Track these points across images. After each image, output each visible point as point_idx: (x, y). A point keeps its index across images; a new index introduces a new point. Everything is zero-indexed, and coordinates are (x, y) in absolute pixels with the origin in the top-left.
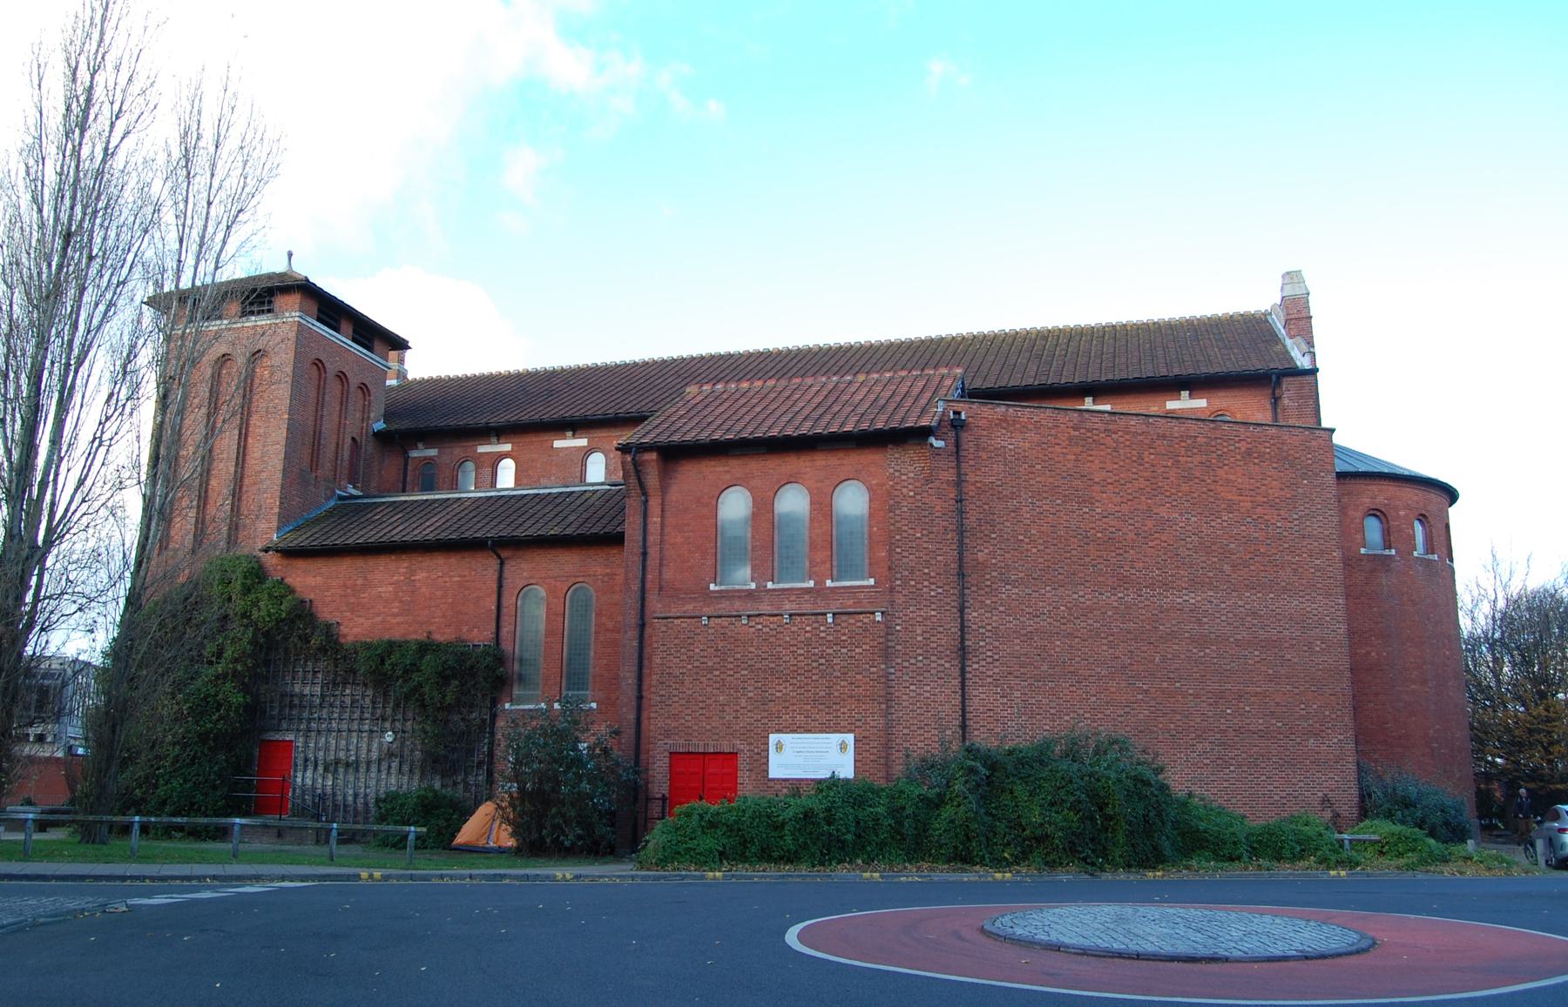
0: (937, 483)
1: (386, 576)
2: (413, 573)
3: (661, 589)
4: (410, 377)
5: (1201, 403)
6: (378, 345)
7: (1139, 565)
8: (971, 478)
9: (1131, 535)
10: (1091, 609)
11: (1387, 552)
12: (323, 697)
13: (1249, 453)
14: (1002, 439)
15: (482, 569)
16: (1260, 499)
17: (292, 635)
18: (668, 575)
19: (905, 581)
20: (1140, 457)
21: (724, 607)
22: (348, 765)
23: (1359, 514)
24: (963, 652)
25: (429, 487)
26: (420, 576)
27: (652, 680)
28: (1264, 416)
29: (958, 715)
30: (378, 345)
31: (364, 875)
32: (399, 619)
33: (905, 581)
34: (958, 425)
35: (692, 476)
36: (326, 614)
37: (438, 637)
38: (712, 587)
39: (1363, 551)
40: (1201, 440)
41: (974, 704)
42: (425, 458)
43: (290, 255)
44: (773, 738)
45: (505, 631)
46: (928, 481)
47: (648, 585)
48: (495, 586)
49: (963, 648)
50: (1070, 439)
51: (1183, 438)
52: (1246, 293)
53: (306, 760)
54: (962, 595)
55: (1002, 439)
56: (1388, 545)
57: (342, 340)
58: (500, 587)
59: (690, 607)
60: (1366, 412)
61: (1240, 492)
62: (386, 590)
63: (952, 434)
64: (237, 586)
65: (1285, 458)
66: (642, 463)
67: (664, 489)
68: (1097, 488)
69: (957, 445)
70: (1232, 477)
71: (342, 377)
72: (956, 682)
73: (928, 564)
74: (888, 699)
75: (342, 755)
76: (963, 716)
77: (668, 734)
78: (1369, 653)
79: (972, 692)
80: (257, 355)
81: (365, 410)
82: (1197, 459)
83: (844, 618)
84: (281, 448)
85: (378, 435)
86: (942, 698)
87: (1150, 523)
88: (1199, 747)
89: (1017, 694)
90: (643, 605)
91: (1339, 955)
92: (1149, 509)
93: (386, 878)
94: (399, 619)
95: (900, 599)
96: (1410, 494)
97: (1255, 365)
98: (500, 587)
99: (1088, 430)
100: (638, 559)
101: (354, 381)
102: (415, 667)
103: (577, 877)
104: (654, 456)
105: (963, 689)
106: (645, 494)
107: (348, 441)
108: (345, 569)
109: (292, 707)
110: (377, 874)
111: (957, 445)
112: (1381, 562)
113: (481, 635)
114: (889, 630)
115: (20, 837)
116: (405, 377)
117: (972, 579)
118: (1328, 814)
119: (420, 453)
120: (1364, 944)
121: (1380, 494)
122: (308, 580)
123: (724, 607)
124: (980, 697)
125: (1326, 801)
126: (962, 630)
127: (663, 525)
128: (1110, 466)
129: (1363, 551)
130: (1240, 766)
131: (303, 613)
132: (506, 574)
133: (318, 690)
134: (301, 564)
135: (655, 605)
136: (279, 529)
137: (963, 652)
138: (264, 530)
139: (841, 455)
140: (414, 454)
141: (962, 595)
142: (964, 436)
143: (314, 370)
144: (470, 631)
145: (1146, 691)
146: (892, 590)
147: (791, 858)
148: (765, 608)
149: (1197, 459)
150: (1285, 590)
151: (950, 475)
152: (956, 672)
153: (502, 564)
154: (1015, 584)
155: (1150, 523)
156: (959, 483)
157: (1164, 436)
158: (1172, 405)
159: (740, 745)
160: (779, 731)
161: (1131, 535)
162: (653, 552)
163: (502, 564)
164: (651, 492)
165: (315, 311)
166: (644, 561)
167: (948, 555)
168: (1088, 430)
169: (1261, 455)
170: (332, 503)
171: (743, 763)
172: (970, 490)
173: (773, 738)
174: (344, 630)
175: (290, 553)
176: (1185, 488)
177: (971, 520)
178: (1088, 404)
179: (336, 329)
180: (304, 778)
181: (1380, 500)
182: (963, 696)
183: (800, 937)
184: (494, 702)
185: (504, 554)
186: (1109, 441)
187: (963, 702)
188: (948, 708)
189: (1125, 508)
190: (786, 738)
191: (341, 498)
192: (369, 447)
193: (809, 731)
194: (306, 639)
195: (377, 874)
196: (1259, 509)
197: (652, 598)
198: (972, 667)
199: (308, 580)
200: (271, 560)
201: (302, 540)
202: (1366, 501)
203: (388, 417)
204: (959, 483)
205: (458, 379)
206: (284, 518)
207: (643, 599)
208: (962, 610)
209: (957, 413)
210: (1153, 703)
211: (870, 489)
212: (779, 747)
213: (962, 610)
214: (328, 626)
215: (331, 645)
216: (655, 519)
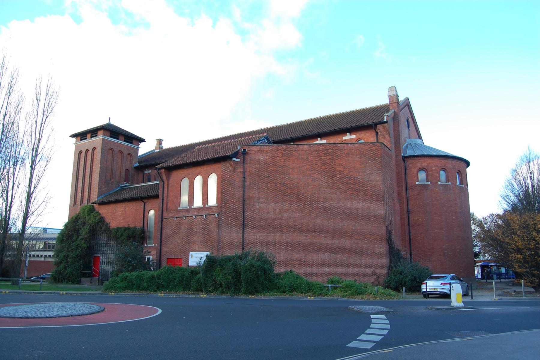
0: (237, 172)
1: (120, 208)
4: (164, 148)
5: (354, 136)
8: (248, 170)
9: (303, 185)
12: (106, 244)
13: (348, 153)
14: (259, 157)
17: (98, 227)
18: (169, 205)
19: (226, 204)
20: (307, 158)
21: (181, 214)
23: (416, 170)
24: (243, 225)
25: (149, 181)
27: (164, 236)
28: (373, 139)
29: (241, 245)
31: (4, 292)
33: (226, 204)
34: (244, 153)
35: (176, 174)
36: (107, 220)
37: (131, 226)
39: (417, 183)
43: (110, 118)
45: (145, 223)
48: (143, 210)
49: (243, 225)
51: (323, 151)
52: (368, 96)
56: (448, 181)
57: (121, 142)
58: (144, 211)
60: (437, 134)
64: (86, 214)
67: (168, 180)
68: (291, 170)
69: (244, 160)
71: (121, 152)
76: (243, 246)
77: (166, 253)
78: (418, 219)
79: (246, 238)
80: (94, 149)
82: (329, 157)
84: (98, 175)
86: (236, 240)
87: (310, 180)
89: (261, 238)
90: (162, 215)
92: (310, 175)
93: (9, 293)
95: (224, 210)
96: (438, 162)
97: (389, 122)
98: (144, 211)
101: (125, 153)
103: (67, 293)
104: (163, 170)
106: (163, 182)
107: (124, 170)
108: (111, 207)
110: (7, 292)
111: (244, 160)
112: (425, 187)
113: (140, 225)
115: (39, 283)
117: (247, 202)
118: (375, 277)
120: (102, 309)
121: (423, 162)
122: (105, 211)
124: (249, 240)
125: (374, 272)
126: (243, 218)
127: (168, 190)
128: (296, 162)
129: (417, 183)
130: (341, 260)
131: (102, 220)
132: (146, 207)
134: (102, 207)
135: (165, 214)
137: (243, 225)
138: (95, 197)
139: (210, 166)
140: (146, 172)
142: (246, 156)
147: (146, 289)
148: (190, 214)
149: (329, 157)
153: (145, 204)
154: (262, 203)
155: (310, 180)
156: (244, 172)
157: (316, 151)
158: (345, 138)
159: (183, 256)
161: (303, 185)
162: (165, 199)
163: (145, 204)
166: (163, 202)
167: (240, 195)
169: (352, 154)
170: (119, 188)
171: (183, 261)
172: (248, 174)
174: (111, 225)
175: (100, 204)
176: (323, 167)
177: (248, 183)
179: (118, 139)
180: (102, 267)
183: (158, 311)
186: (296, 154)
188: (239, 243)
191: (121, 187)
192: (132, 172)
193: (199, 251)
194: (101, 228)
195: (64, 293)
196: (351, 173)
197: (165, 212)
200: (96, 206)
202: (419, 165)
203: (139, 163)
204: (244, 172)
205: (174, 148)
206: (99, 194)
207: (162, 213)
208: (244, 212)
209: (244, 150)
210: (309, 240)
211: (217, 176)
212: (192, 256)
213: (244, 212)
214: (107, 224)
215: (108, 229)
216: (166, 189)
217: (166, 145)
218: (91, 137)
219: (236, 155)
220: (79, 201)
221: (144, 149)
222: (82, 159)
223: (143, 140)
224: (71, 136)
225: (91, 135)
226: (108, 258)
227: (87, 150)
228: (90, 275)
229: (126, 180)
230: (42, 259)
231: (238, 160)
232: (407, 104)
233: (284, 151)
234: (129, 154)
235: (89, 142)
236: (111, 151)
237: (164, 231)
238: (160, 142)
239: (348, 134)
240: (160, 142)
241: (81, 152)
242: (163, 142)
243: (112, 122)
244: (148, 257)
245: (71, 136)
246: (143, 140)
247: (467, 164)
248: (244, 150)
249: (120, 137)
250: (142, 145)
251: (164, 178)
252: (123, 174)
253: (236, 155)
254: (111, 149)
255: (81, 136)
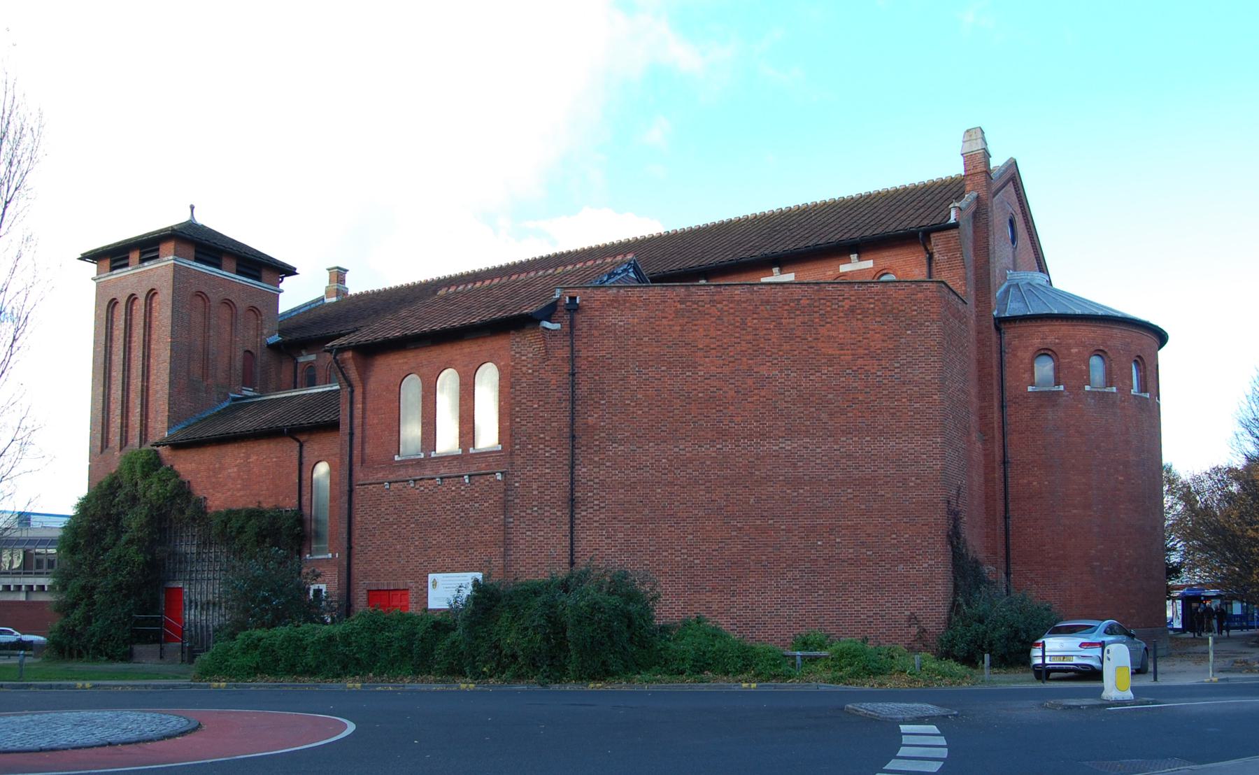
0: (553, 360)
1: (233, 459)
2: (248, 457)
3: (363, 462)
6: (265, 274)
7: (736, 419)
8: (583, 353)
9: (732, 393)
10: (691, 461)
11: (1056, 388)
12: (199, 553)
13: (852, 310)
14: (614, 318)
15: (284, 451)
16: (861, 351)
20: (744, 323)
21: (402, 474)
22: (214, 604)
23: (1027, 356)
24: (572, 502)
25: (312, 383)
26: (253, 458)
28: (919, 273)
30: (265, 274)
32: (242, 493)
34: (573, 308)
35: (385, 366)
36: (199, 491)
37: (265, 506)
38: (396, 458)
39: (1030, 389)
40: (804, 302)
41: (581, 545)
42: (309, 363)
43: (192, 208)
44: (431, 577)
45: (305, 498)
46: (545, 360)
47: (355, 459)
50: (676, 312)
52: (917, 157)
53: (191, 602)
54: (573, 455)
55: (614, 318)
56: (1109, 383)
57: (227, 274)
58: (301, 464)
59: (380, 475)
61: (842, 346)
62: (233, 471)
63: (567, 317)
64: (139, 474)
65: (890, 312)
66: (343, 361)
68: (700, 354)
69: (572, 326)
70: (834, 334)
71: (228, 303)
72: (567, 527)
73: (543, 430)
74: (507, 543)
75: (211, 597)
76: (572, 555)
78: (1030, 483)
80: (152, 294)
81: (259, 328)
83: (477, 478)
85: (273, 347)
86: (554, 541)
87: (750, 382)
88: (790, 575)
91: (151, 740)
92: (750, 369)
94: (242, 493)
98: (301, 464)
99: (694, 303)
100: (347, 438)
101: (242, 306)
102: (241, 530)
103: (95, 686)
105: (572, 533)
107: (240, 354)
109: (181, 562)
111: (572, 326)
113: (290, 503)
114: (507, 486)
116: (345, 293)
119: (306, 358)
122: (189, 465)
123: (402, 474)
124: (586, 540)
125: (912, 619)
126: (572, 484)
127: (364, 410)
129: (1030, 389)
131: (183, 491)
132: (305, 454)
133: (194, 549)
134: (182, 454)
135: (359, 474)
136: (169, 428)
137: (572, 502)
138: (160, 428)
139: (480, 342)
140: (301, 360)
141: (573, 455)
142: (579, 317)
143: (190, 297)
144: (284, 499)
145: (740, 529)
146: (511, 453)
147: (311, 672)
149: (799, 320)
150: (881, 433)
151: (565, 353)
152: (567, 519)
153: (301, 446)
155: (750, 382)
156: (573, 359)
157: (768, 302)
158: (844, 268)
160: (435, 572)
162: (357, 432)
163: (301, 446)
164: (355, 384)
165: (192, 253)
168: (694, 303)
170: (226, 404)
171: (412, 597)
172: (582, 364)
173: (431, 577)
174: (210, 503)
175: (177, 446)
176: (786, 347)
177: (583, 390)
178: (777, 276)
180: (190, 615)
181: (1051, 340)
182: (572, 539)
184: (300, 553)
185: (303, 438)
186: (713, 311)
187: (572, 544)
189: (726, 370)
190: (439, 577)
191: (235, 399)
193: (453, 571)
194: (182, 512)
195: (88, 684)
196: (860, 362)
197: (357, 468)
198: (581, 513)
199: (189, 465)
200: (123, 453)
201: (181, 437)
202: (1037, 342)
203: (281, 332)
204: (573, 359)
206: (173, 420)
208: (572, 468)
209: (573, 299)
210: (746, 538)
211: (500, 370)
212: (435, 584)
213: (572, 468)
215: (201, 511)
216: (358, 406)
217: (356, 285)
218: (142, 261)
219: (550, 312)
220: (115, 439)
221: (293, 296)
222: (118, 323)
223: (291, 271)
224: (84, 257)
225: (142, 254)
226: (204, 594)
227: (132, 298)
228: (157, 638)
229: (248, 381)
230: (22, 597)
231: (557, 326)
232: (1012, 176)
233: (681, 302)
234: (253, 309)
235: (134, 275)
236: (199, 301)
237: (357, 518)
238: (339, 275)
239: (854, 257)
240: (339, 275)
241: (113, 303)
242: (348, 277)
243: (201, 220)
244: (313, 587)
245: (84, 257)
246: (291, 271)
247: (1161, 337)
248: (573, 299)
249: (226, 262)
250: (287, 283)
251: (353, 374)
252: (239, 364)
253: (550, 312)
254: (200, 294)
255: (112, 257)
